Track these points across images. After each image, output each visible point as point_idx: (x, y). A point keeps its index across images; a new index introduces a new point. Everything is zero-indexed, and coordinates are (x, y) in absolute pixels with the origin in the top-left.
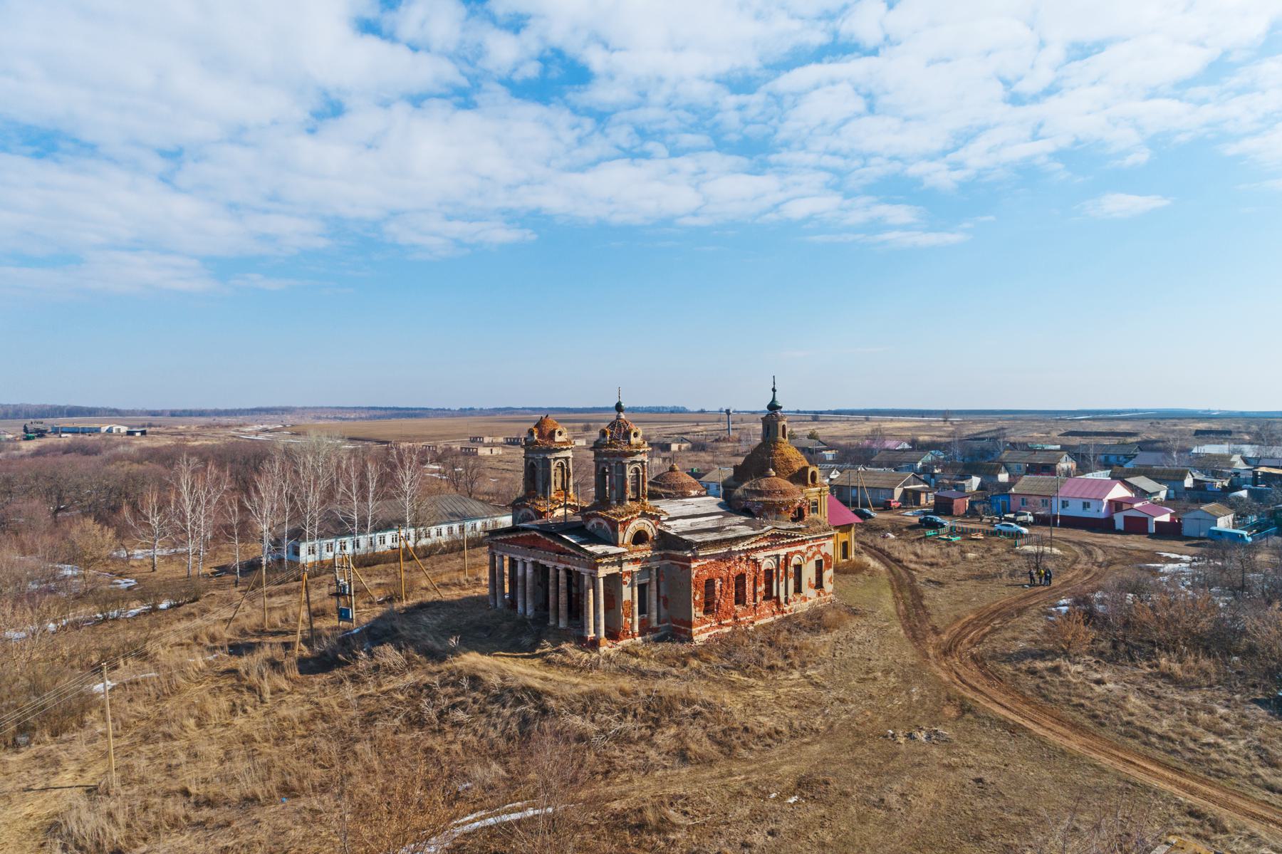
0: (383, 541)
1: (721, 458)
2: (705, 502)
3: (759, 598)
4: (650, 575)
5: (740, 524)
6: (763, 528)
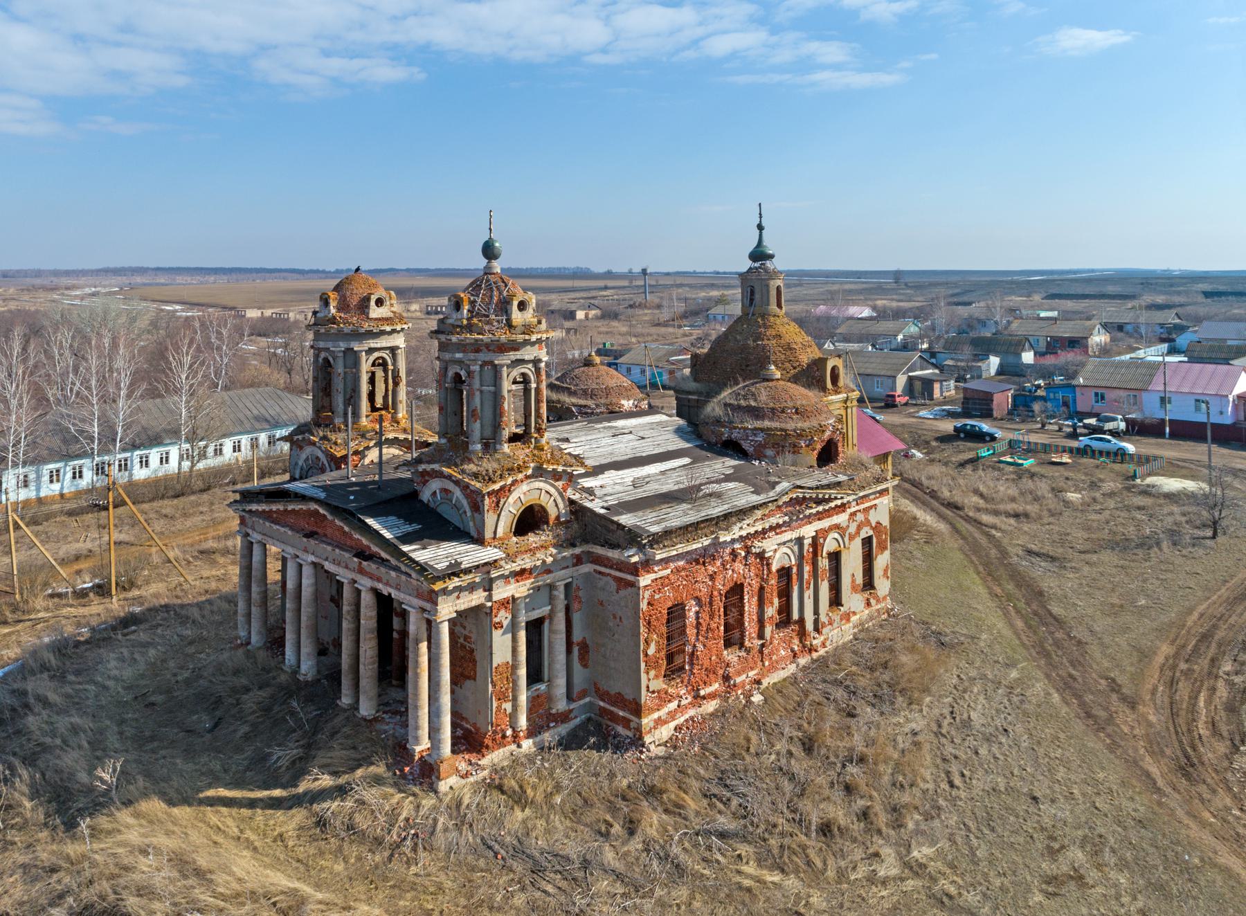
0: (145, 462)
1: (639, 329)
2: (652, 426)
3: (768, 630)
4: (552, 599)
5: (728, 479)
6: (773, 485)
